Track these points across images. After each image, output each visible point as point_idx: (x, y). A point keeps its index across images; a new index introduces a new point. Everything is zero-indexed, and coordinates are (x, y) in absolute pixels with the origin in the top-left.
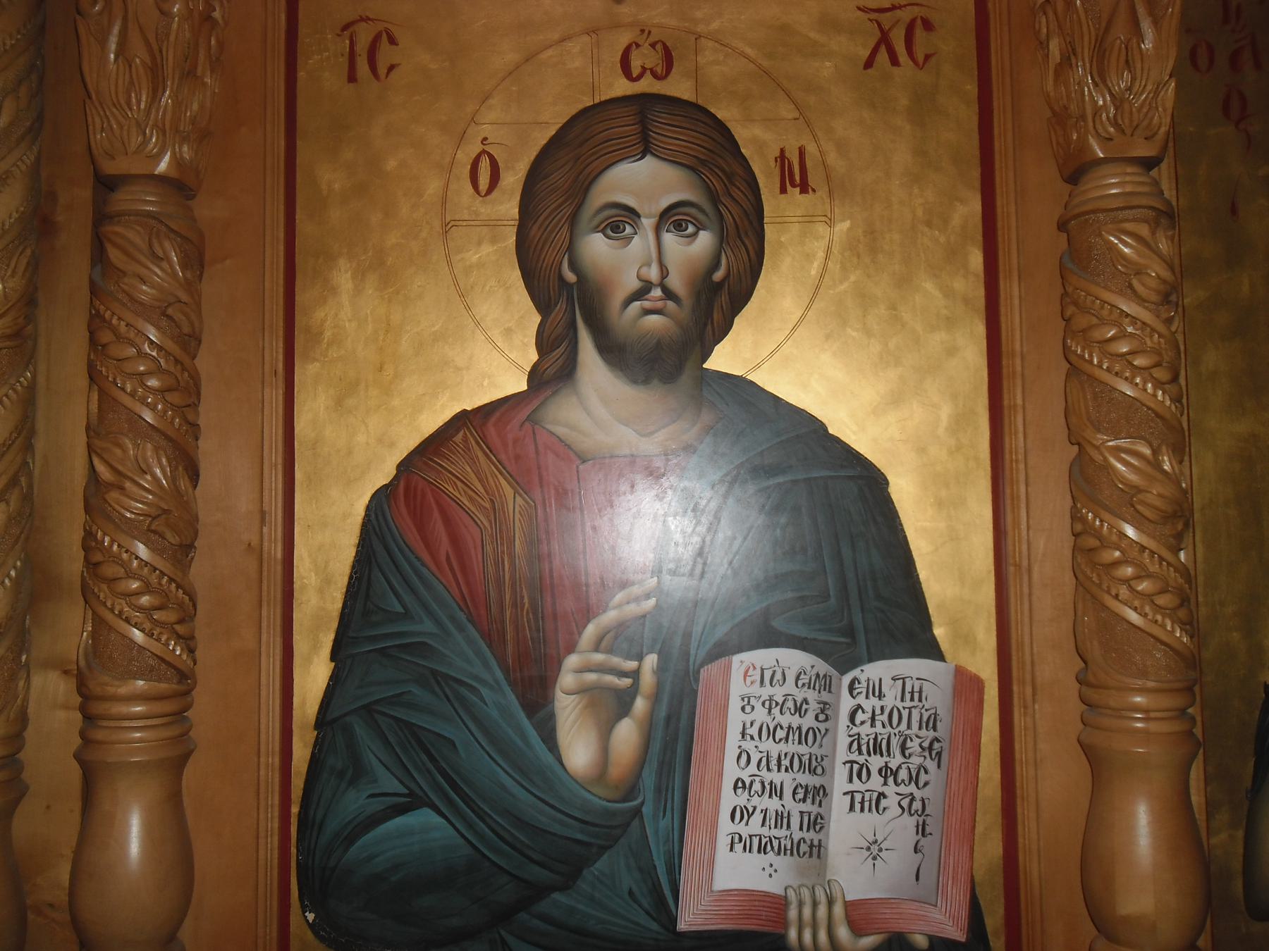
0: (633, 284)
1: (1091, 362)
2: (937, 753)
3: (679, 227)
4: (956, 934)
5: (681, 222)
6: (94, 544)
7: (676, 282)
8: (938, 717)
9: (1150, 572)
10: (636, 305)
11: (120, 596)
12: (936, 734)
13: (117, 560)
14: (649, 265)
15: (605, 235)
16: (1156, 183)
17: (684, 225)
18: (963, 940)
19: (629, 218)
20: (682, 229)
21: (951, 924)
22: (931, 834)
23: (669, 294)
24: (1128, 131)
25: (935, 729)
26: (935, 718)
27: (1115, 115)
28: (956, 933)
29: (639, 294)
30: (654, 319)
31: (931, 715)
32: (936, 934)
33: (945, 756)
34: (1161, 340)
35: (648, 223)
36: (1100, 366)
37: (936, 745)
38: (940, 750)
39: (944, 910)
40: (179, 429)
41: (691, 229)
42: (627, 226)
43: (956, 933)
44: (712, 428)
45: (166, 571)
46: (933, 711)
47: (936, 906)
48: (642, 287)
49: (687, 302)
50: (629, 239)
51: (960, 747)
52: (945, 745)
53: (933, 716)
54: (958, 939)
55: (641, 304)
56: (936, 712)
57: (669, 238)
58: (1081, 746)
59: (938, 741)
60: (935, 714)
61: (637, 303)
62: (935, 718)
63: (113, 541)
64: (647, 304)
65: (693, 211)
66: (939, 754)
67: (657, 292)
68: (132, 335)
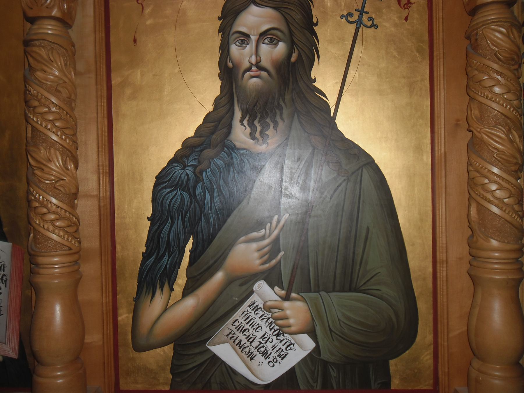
0: (246, 65)
1: (37, 122)
2: (5, 281)
4: (14, 355)
6: (33, 198)
7: (265, 63)
8: (5, 266)
10: (248, 74)
12: (4, 273)
13: (42, 205)
14: (251, 56)
18: (16, 358)
21: (12, 352)
22: (3, 314)
23: (261, 68)
25: (4, 270)
26: (4, 266)
28: (13, 354)
30: (254, 80)
31: (2, 265)
32: (6, 356)
33: (8, 282)
36: (41, 125)
37: (4, 277)
38: (6, 279)
39: (8, 346)
40: (69, 143)
41: (275, 41)
42: (246, 41)
43: (13, 354)
45: (63, 207)
46: (3, 263)
47: (5, 344)
51: (14, 278)
52: (8, 277)
53: (3, 265)
54: (14, 357)
55: (250, 73)
56: (4, 263)
57: (265, 47)
59: (5, 276)
60: (4, 264)
61: (248, 73)
62: (4, 266)
63: (40, 196)
64: (252, 73)
66: (6, 281)
68: (47, 103)
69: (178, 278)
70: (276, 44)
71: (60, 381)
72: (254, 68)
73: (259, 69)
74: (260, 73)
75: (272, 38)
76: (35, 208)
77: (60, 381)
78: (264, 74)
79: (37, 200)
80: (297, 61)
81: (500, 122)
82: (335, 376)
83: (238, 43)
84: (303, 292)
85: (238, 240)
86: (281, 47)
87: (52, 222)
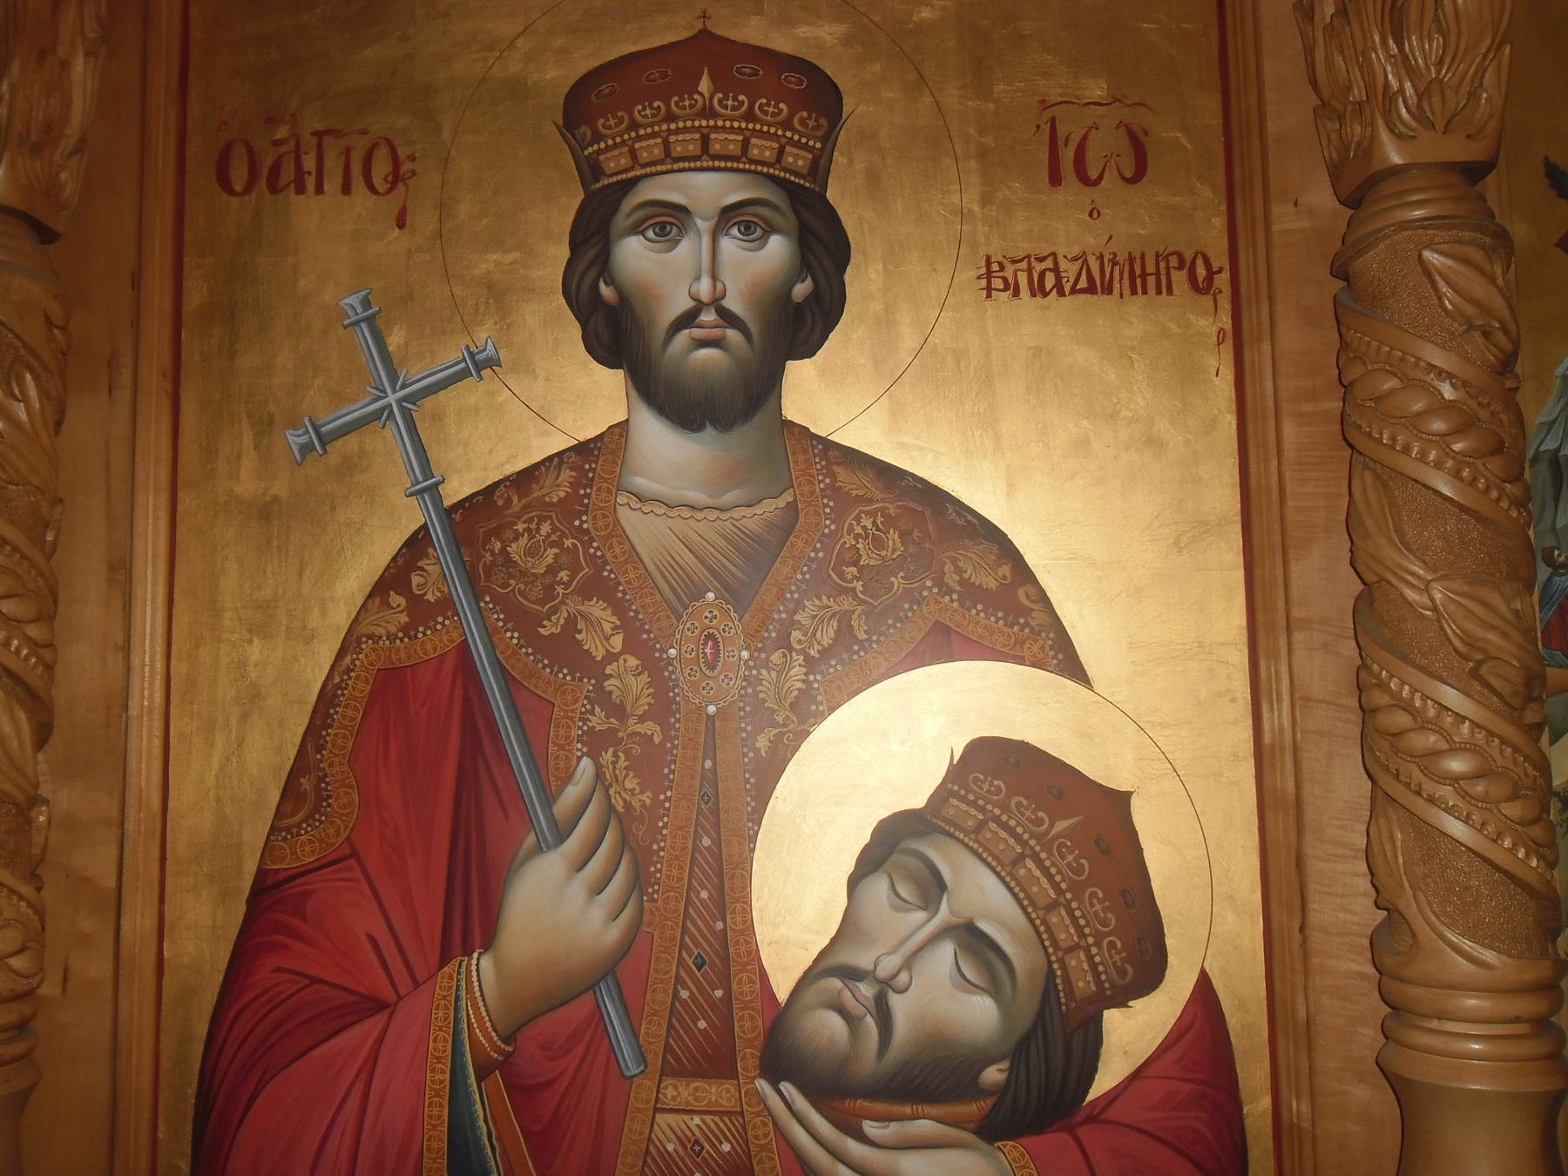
0: (683, 304)
3: (747, 228)
5: (751, 224)
7: (733, 304)
9: (1453, 786)
11: (1443, 781)
14: (698, 278)
15: (645, 238)
16: (1482, 198)
17: (753, 228)
19: (673, 217)
20: (666, 232)
23: (728, 318)
24: (1440, 125)
27: (1419, 106)
29: (687, 320)
34: (1368, 430)
35: (703, 225)
41: (759, 232)
44: (1176, 524)
48: (693, 308)
49: (754, 328)
50: (677, 242)
57: (730, 246)
58: (1387, 1078)
64: (698, 333)
65: (764, 211)
67: (709, 317)
69: (1244, 644)
70: (763, 240)
71: (1477, 1047)
72: (709, 317)
73: (728, 323)
74: (725, 332)
75: (750, 221)
76: (1513, 797)
77: (1477, 1047)
78: (732, 335)
79: (1383, 686)
80: (807, 299)
81: (1409, 295)
82: (804, 672)
83: (650, 234)
84: (409, 669)
85: (23, 709)
86: (777, 249)
87: (1455, 750)
